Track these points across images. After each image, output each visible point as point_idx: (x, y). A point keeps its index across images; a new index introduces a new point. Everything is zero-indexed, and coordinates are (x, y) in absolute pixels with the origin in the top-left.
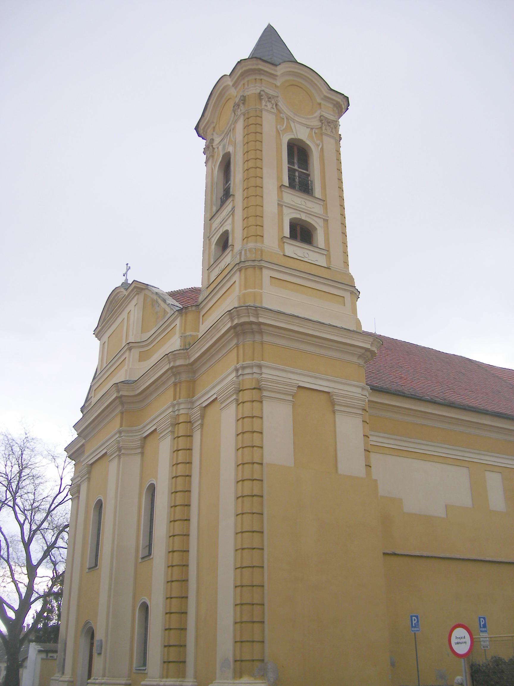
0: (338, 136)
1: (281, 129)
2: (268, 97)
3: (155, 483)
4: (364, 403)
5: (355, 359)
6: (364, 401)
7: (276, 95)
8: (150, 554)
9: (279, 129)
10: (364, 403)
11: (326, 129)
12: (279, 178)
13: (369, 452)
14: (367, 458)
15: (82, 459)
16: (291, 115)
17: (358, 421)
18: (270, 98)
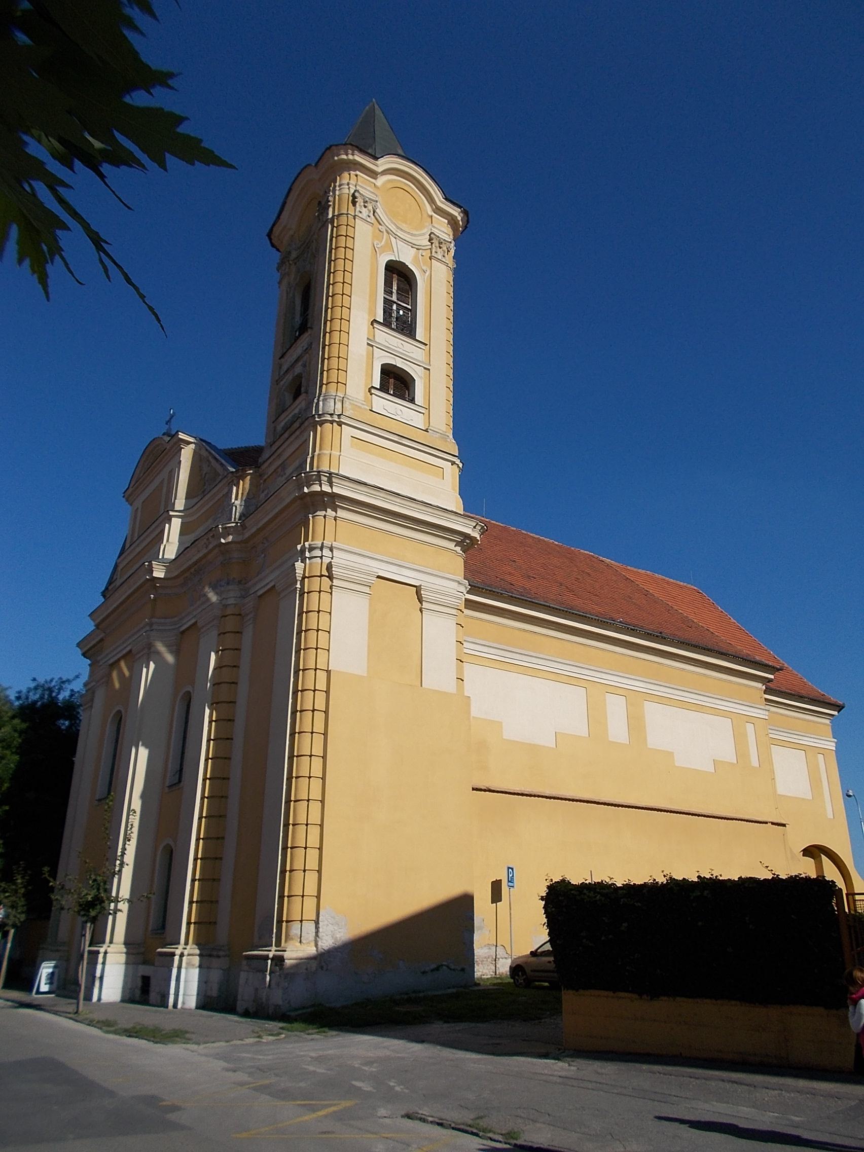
0: (179, 461)
1: (378, 246)
2: (364, 200)
3: (191, 691)
4: (460, 602)
5: (451, 545)
6: (460, 599)
7: (374, 199)
8: (180, 781)
9: (375, 246)
10: (460, 602)
11: (436, 252)
12: (372, 311)
13: (462, 662)
14: (460, 670)
15: (99, 658)
16: (393, 228)
17: (451, 623)
18: (367, 202)
